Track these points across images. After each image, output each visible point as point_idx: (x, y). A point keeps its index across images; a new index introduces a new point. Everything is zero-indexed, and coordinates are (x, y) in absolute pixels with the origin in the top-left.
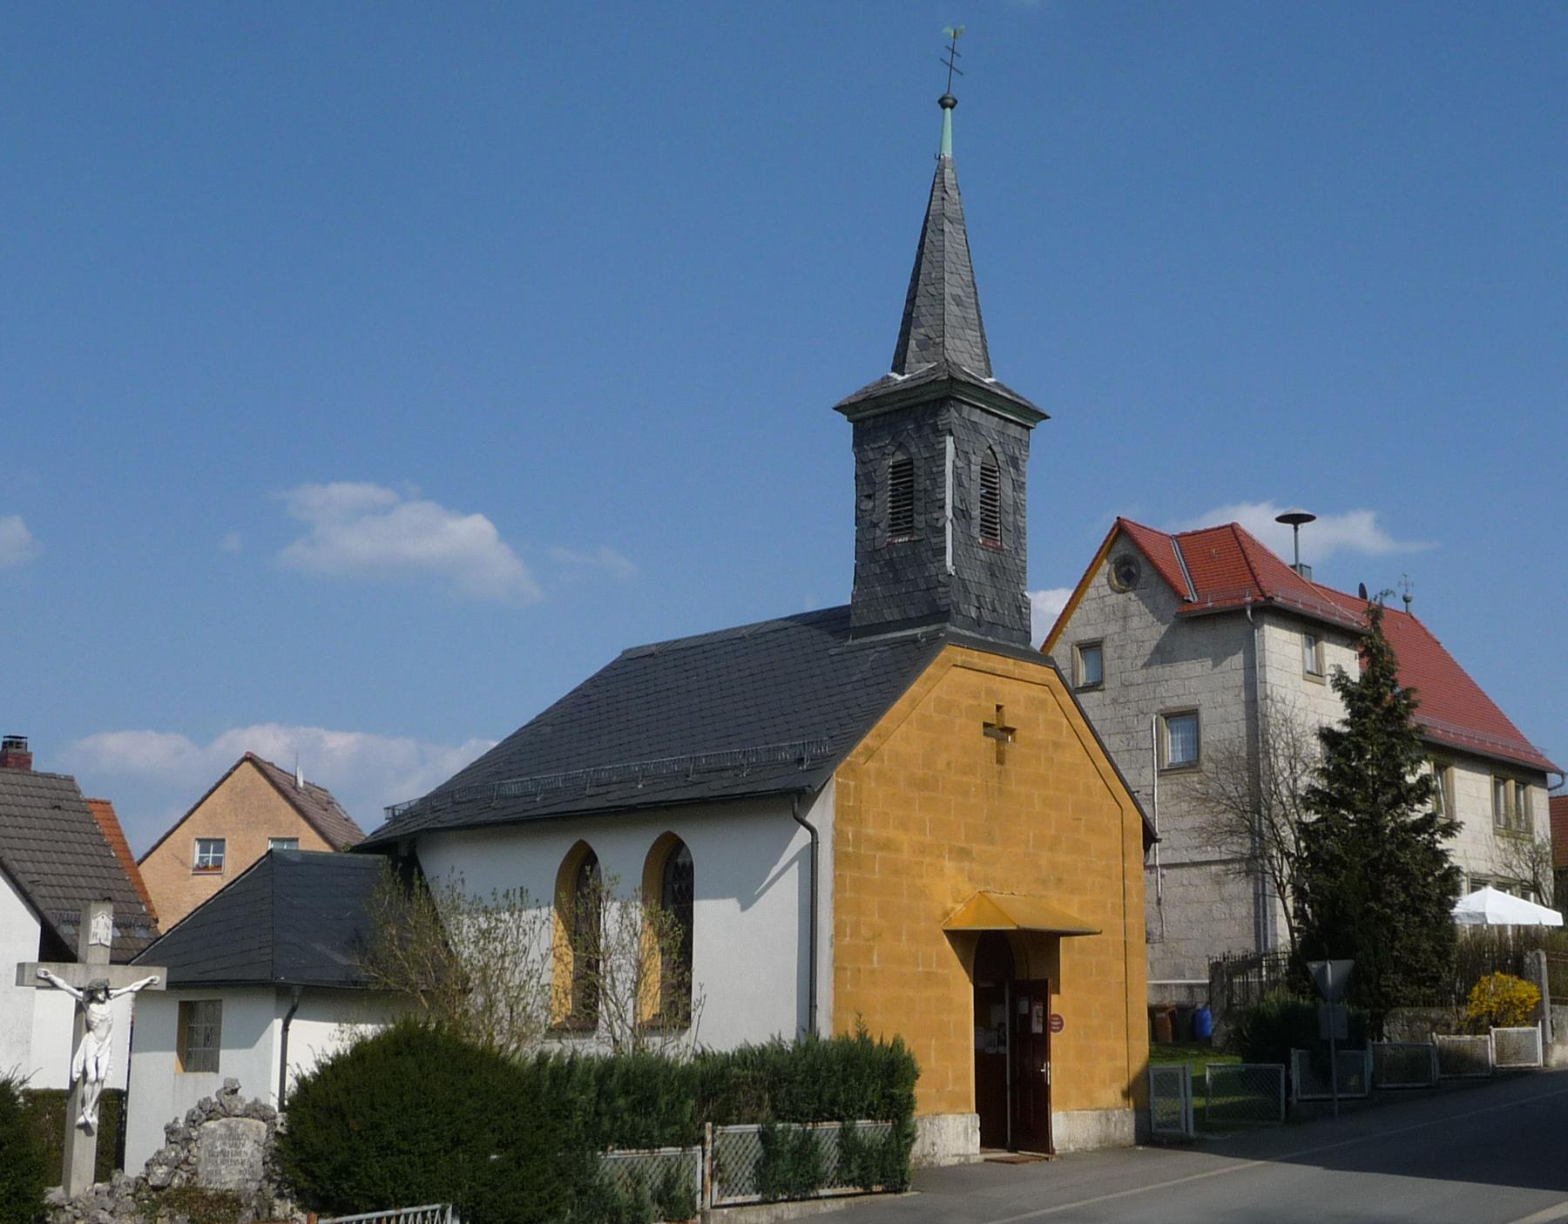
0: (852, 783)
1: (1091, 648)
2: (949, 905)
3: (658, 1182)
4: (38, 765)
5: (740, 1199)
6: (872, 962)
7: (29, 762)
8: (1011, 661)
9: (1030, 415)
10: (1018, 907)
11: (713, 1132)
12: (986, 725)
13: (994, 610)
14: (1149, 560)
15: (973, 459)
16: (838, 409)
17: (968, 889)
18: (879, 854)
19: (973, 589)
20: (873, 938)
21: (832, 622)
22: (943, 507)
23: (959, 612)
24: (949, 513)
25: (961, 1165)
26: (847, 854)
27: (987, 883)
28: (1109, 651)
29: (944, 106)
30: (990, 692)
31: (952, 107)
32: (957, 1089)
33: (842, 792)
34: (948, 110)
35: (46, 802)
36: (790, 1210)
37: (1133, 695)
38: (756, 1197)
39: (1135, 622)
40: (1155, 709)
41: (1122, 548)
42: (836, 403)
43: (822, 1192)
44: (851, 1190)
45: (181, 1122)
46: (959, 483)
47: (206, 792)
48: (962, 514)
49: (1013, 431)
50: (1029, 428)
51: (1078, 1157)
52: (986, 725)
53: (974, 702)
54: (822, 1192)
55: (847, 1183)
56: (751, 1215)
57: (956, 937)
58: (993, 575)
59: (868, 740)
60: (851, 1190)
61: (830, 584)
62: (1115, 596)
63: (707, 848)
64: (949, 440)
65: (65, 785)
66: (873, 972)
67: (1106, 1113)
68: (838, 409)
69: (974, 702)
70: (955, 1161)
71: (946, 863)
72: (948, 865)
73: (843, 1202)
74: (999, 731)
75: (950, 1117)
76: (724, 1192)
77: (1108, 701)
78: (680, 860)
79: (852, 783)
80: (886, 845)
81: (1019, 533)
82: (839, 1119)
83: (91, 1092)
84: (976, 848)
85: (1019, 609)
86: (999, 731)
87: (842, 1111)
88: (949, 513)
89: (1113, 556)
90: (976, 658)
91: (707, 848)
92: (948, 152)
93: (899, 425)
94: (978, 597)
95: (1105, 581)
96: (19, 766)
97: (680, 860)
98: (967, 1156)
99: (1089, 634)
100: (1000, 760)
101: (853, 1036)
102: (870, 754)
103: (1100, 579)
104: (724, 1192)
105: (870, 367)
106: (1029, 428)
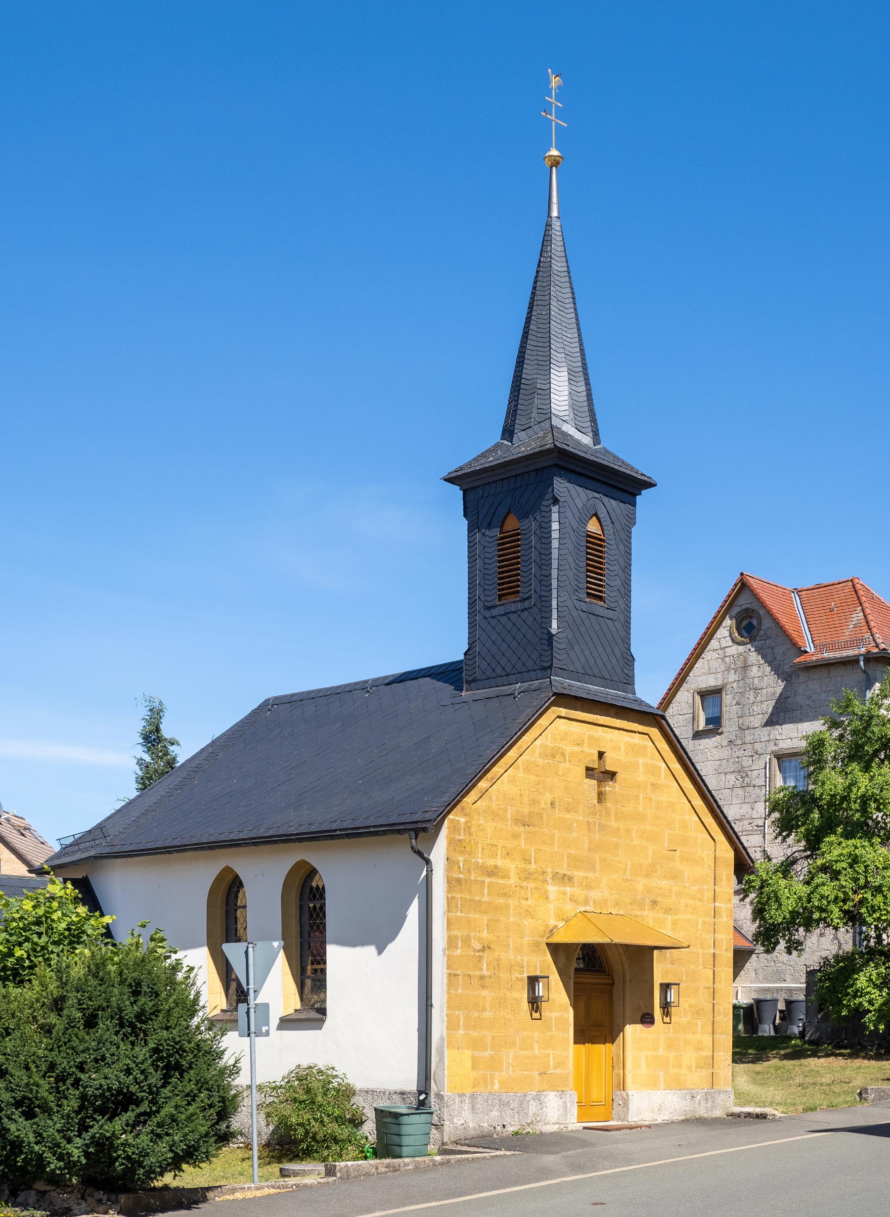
0: (462, 820)
1: (710, 696)
6: (481, 969)
9: (624, 486)
12: (588, 769)
14: (769, 612)
16: (449, 480)
18: (488, 880)
21: (448, 674)
28: (727, 699)
32: (558, 1071)
33: (455, 828)
37: (748, 739)
39: (754, 671)
40: (769, 750)
41: (744, 601)
42: (445, 474)
47: (835, 673)
52: (588, 769)
61: (450, 644)
62: (735, 647)
63: (342, 875)
65: (631, 659)
66: (482, 978)
69: (577, 749)
72: (552, 889)
74: (602, 774)
77: (725, 743)
78: (314, 884)
80: (493, 872)
83: (287, 1110)
84: (578, 874)
86: (602, 774)
89: (735, 610)
91: (342, 875)
93: (509, 494)
95: (727, 634)
97: (314, 884)
99: (711, 682)
100: (601, 797)
103: (723, 632)
105: (479, 439)
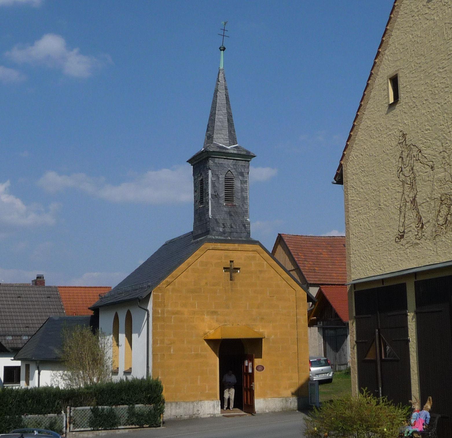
0: (160, 294)
2: (207, 330)
3: (47, 424)
4: (46, 284)
5: (82, 429)
6: (170, 352)
7: (44, 283)
8: (236, 245)
10: (236, 331)
11: (70, 409)
13: (232, 227)
15: (220, 176)
16: (187, 162)
17: (216, 325)
18: (173, 316)
19: (221, 222)
20: (171, 344)
22: (208, 195)
23: (214, 230)
24: (210, 196)
25: (211, 417)
26: (158, 317)
27: (226, 322)
29: (221, 50)
30: (226, 257)
31: (224, 50)
34: (222, 51)
35: (46, 296)
36: (103, 433)
38: (89, 429)
43: (119, 427)
44: (134, 426)
45: (86, 393)
46: (214, 186)
48: (216, 196)
49: (243, 163)
50: (249, 161)
51: (263, 415)
53: (219, 261)
54: (119, 427)
55: (132, 424)
56: (85, 434)
57: (210, 342)
58: (231, 215)
59: (168, 279)
60: (134, 426)
64: (210, 172)
67: (286, 399)
68: (187, 162)
70: (209, 416)
71: (206, 317)
72: (207, 317)
73: (127, 431)
74: (231, 270)
75: (206, 402)
76: (74, 427)
79: (160, 294)
80: (177, 313)
81: (244, 199)
82: (127, 404)
85: (244, 226)
86: (231, 270)
87: (130, 402)
88: (210, 196)
90: (219, 246)
92: (222, 67)
94: (223, 224)
96: (41, 284)
98: (215, 415)
101: (50, 386)
102: (169, 284)
104: (74, 427)
106: (249, 161)
